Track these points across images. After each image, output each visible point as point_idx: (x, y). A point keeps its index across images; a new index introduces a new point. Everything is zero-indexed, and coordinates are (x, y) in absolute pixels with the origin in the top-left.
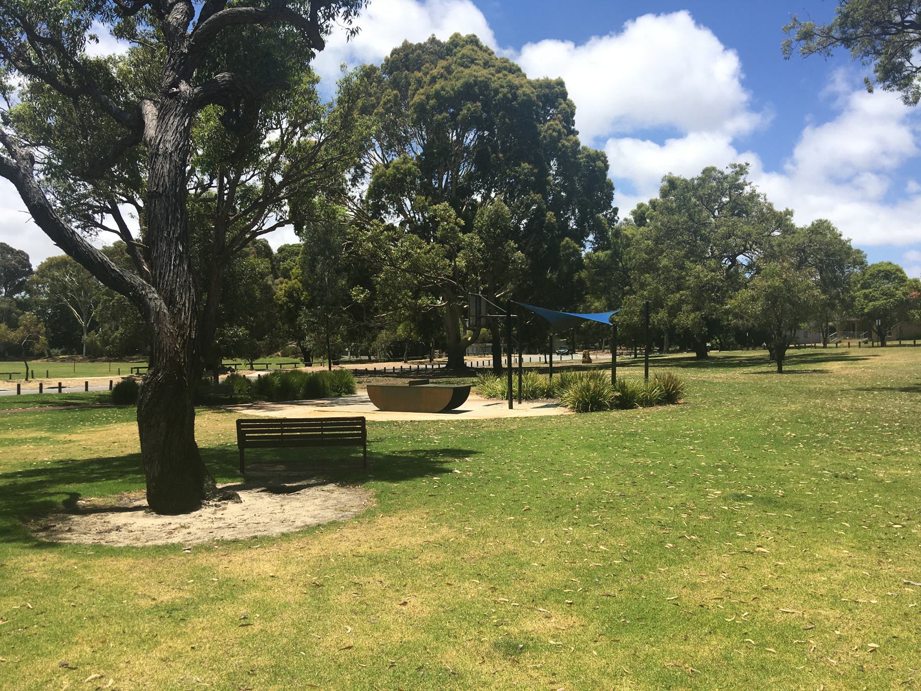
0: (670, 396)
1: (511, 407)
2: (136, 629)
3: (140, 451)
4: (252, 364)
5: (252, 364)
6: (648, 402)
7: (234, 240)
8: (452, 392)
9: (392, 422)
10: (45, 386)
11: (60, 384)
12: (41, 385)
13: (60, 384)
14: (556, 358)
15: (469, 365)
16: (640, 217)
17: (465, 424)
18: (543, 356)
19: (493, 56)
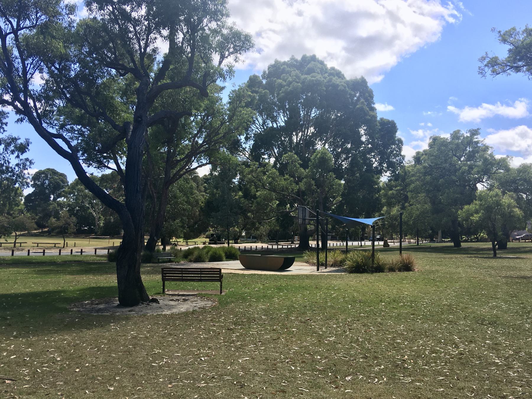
0: (407, 267)
1: (318, 270)
2: (275, 316)
3: (116, 285)
4: (187, 242)
5: (187, 242)
6: (392, 270)
7: (175, 175)
8: (283, 259)
9: (252, 274)
10: (73, 251)
11: (82, 250)
12: (72, 250)
13: (82, 250)
14: (350, 243)
15: (310, 245)
16: (418, 159)
17: (294, 277)
18: (360, 242)
19: (510, 173)
